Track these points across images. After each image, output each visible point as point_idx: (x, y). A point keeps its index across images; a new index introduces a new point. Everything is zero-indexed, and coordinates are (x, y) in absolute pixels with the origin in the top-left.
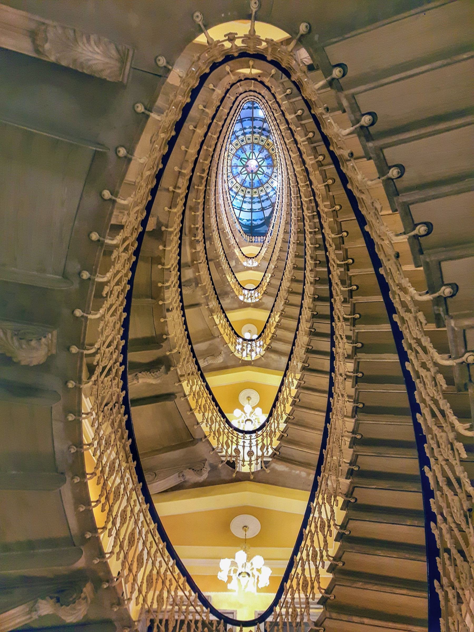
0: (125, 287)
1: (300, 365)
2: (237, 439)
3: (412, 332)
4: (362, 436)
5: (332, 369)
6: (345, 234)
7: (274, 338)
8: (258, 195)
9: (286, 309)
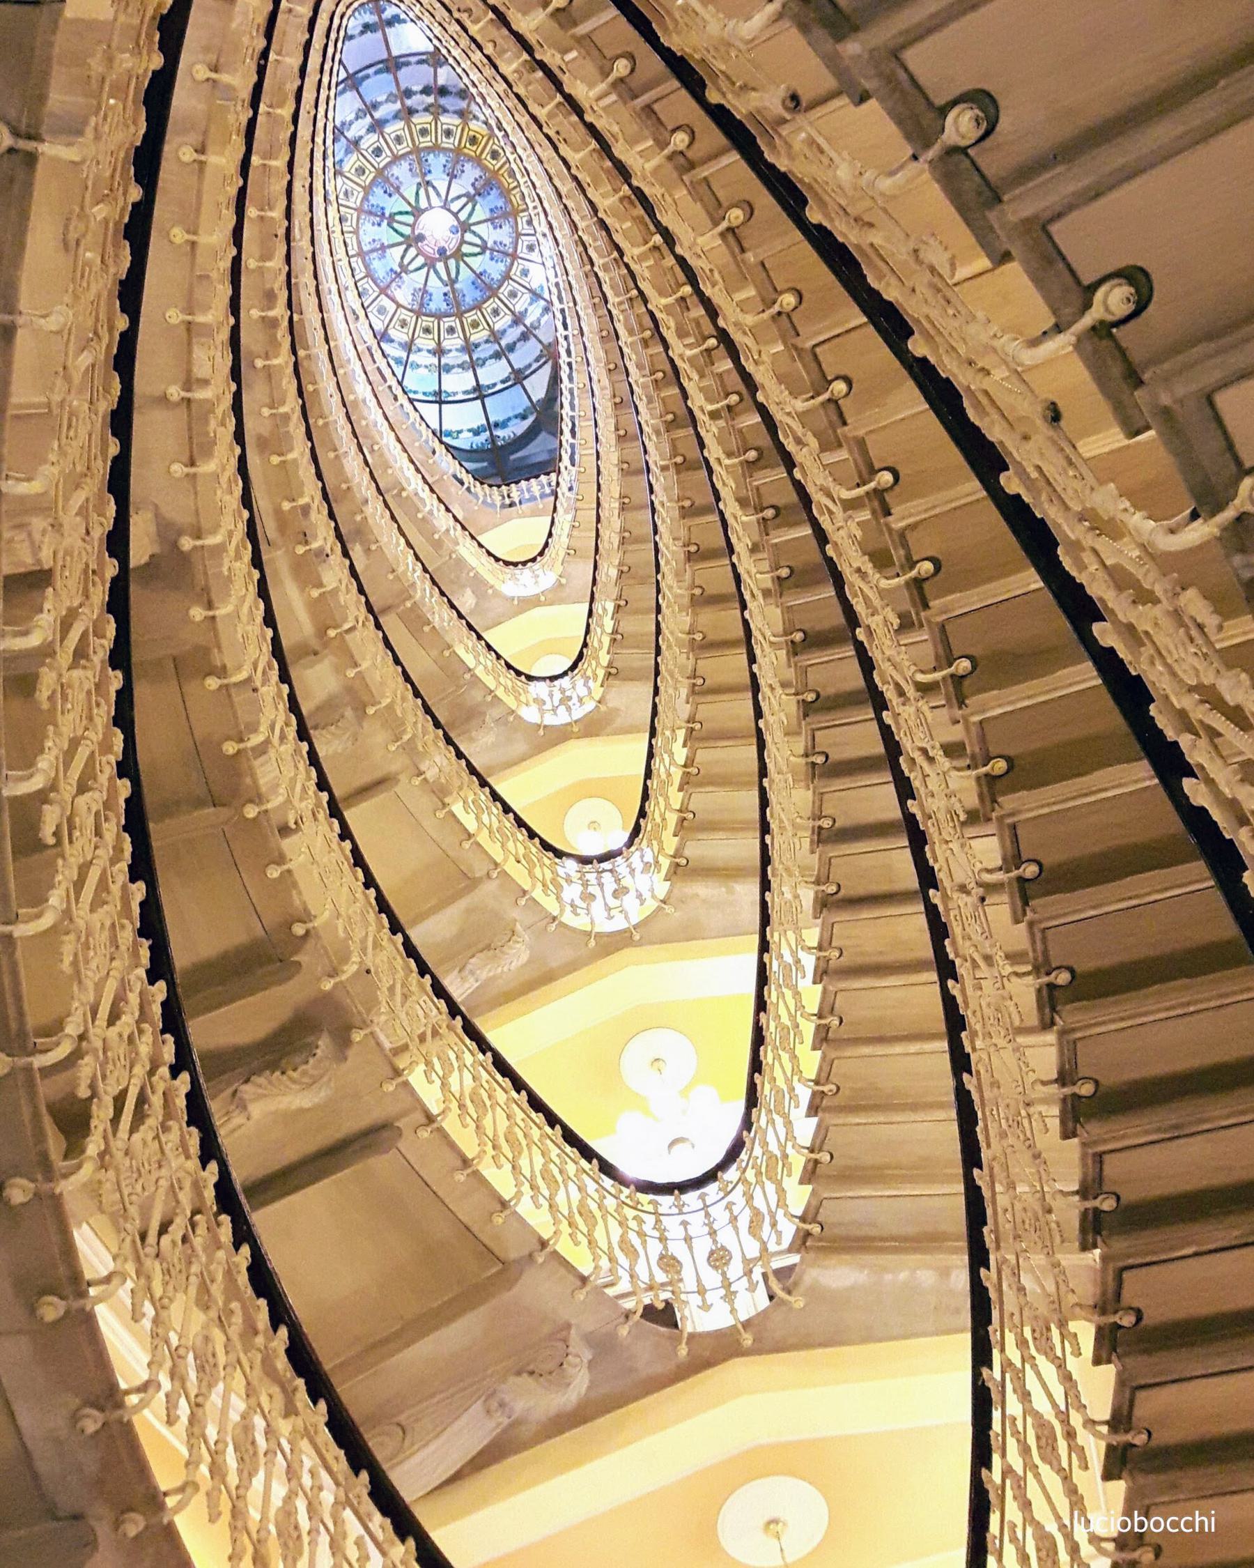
0: (113, 791)
1: (808, 896)
2: (658, 1221)
3: (1176, 667)
4: (1097, 1082)
5: (927, 877)
6: (840, 387)
7: (687, 825)
8: (486, 333)
9: (704, 711)
